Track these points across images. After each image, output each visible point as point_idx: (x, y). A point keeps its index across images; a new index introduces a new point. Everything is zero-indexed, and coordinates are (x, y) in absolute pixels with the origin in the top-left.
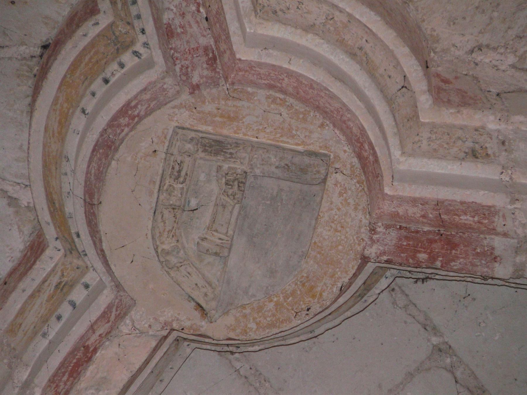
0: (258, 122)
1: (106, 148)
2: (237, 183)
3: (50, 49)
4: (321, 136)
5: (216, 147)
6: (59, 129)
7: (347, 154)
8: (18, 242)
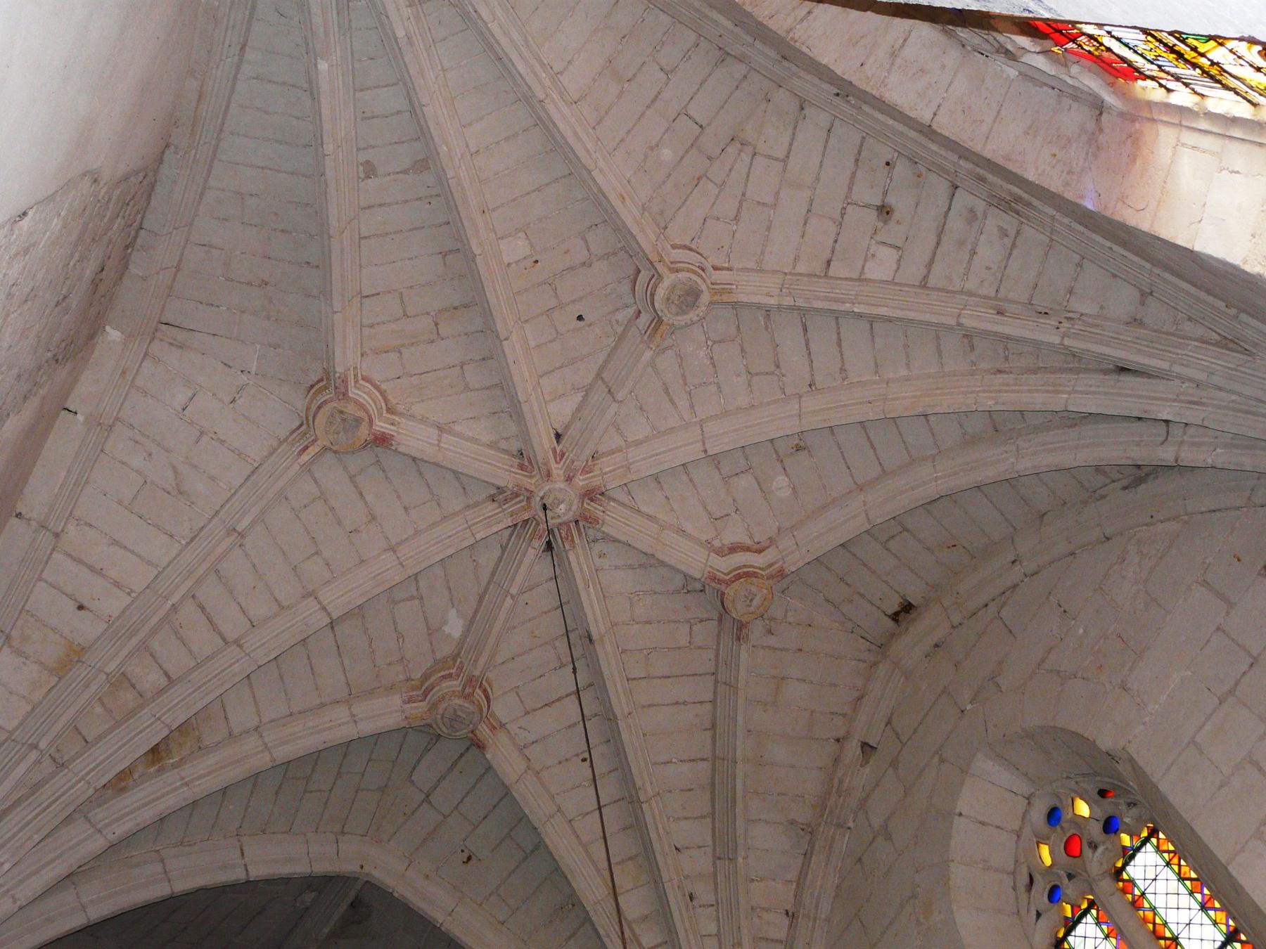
0: (350, 409)
1: (319, 407)
2: (344, 420)
3: (312, 386)
4: (362, 414)
5: (341, 412)
6: (311, 402)
7: (1100, 849)
8: (298, 424)
